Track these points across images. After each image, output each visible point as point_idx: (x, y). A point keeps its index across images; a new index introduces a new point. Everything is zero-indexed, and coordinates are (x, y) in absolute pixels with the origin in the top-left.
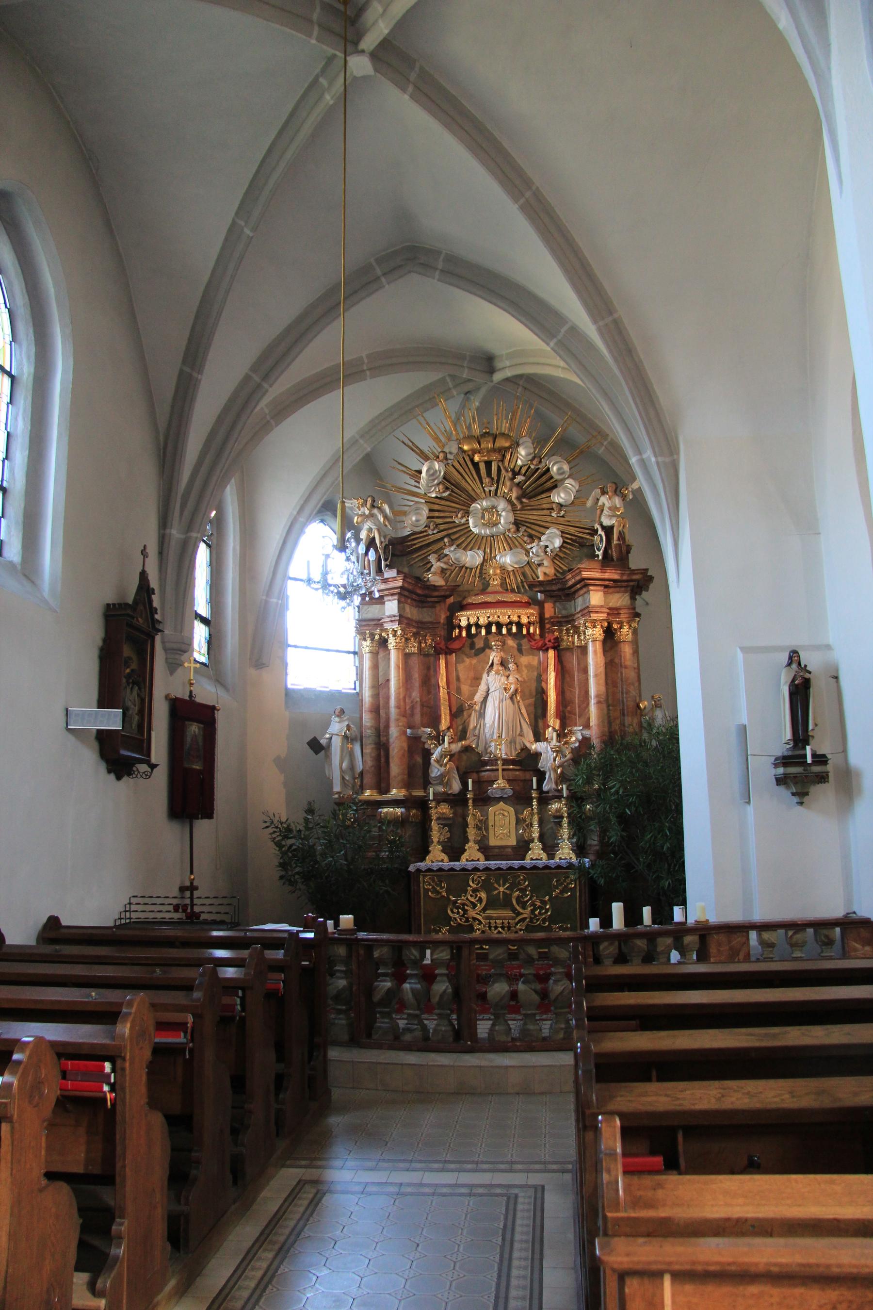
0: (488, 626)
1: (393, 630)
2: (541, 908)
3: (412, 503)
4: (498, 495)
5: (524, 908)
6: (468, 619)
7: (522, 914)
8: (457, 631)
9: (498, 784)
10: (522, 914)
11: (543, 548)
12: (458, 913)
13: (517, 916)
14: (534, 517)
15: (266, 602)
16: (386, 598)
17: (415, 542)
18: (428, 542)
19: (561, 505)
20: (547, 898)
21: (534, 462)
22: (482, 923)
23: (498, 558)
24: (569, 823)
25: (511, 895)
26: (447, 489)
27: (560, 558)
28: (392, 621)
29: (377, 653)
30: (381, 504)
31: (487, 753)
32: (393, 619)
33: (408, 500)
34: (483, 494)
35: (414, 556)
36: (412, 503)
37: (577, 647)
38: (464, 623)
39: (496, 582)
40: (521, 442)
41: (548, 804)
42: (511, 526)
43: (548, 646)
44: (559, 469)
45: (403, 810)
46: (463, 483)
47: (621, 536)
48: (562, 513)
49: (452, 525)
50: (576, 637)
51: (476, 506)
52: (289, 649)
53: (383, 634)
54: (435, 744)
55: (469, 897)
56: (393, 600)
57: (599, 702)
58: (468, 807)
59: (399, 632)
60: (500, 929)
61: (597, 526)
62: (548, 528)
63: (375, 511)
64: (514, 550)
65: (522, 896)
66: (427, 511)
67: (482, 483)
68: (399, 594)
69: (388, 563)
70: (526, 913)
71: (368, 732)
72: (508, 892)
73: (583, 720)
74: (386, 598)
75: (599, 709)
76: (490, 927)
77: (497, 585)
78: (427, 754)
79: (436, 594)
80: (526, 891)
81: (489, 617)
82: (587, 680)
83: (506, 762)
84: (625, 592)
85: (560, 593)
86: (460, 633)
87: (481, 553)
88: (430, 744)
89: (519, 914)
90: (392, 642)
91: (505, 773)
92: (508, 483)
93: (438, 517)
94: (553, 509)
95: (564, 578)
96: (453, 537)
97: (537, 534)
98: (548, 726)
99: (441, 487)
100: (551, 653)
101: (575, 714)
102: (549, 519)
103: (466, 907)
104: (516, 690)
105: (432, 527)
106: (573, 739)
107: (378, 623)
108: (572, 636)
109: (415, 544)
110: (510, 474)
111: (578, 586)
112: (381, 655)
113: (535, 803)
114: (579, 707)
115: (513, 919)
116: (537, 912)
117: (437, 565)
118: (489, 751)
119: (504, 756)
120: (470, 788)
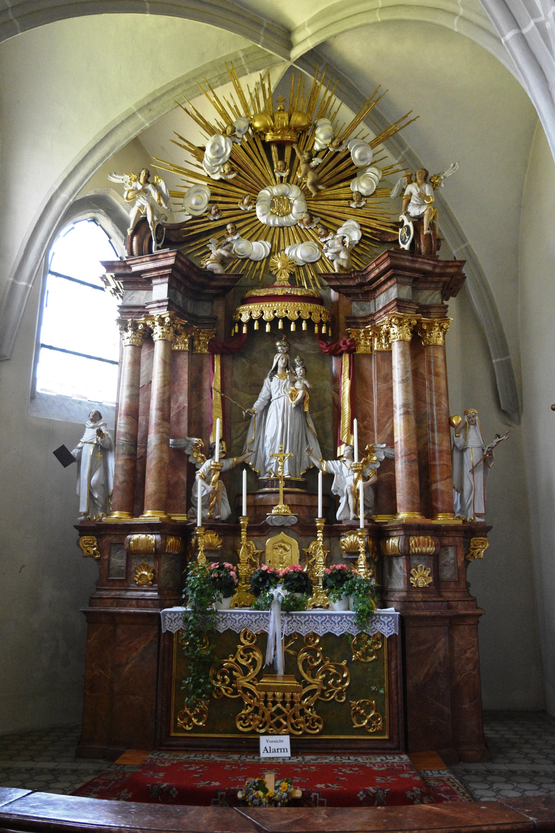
0: (274, 322)
1: (160, 317)
2: (336, 676)
3: (191, 185)
4: (291, 181)
5: (313, 676)
6: (251, 313)
7: (311, 684)
8: (237, 327)
9: (278, 509)
10: (311, 684)
11: (340, 240)
12: (224, 681)
13: (304, 688)
14: (330, 208)
15: (14, 286)
16: (154, 282)
17: (191, 228)
18: (207, 229)
19: (361, 196)
20: (344, 663)
21: (334, 144)
22: (255, 696)
23: (287, 252)
24: (368, 560)
25: (296, 656)
26: (232, 170)
27: (358, 254)
28: (159, 307)
29: (141, 347)
30: (157, 180)
31: (266, 473)
32: (161, 304)
33: (188, 182)
34: (273, 180)
35: (191, 245)
36: (191, 185)
37: (377, 351)
38: (245, 318)
39: (284, 276)
40: (318, 124)
41: (340, 537)
42: (304, 215)
43: (343, 349)
44: (360, 155)
45: (158, 537)
46: (251, 166)
47: (432, 226)
48: (363, 203)
49: (237, 212)
50: (376, 339)
51: (265, 193)
52: (43, 351)
53: (149, 323)
54: (202, 458)
55: (240, 660)
56: (162, 283)
57: (406, 413)
58: (240, 536)
59: (167, 320)
60: (279, 705)
61: (403, 217)
62: (345, 221)
63: (150, 187)
64: (306, 243)
65: (311, 659)
66: (209, 194)
67: (273, 168)
68: (169, 275)
69: (160, 245)
70: (316, 682)
71: (121, 439)
72: (291, 652)
73: (384, 436)
74: (154, 282)
75: (407, 421)
76: (266, 702)
77: (284, 280)
78: (192, 469)
79: (214, 283)
80: (316, 652)
81: (275, 312)
82: (391, 389)
83: (288, 482)
84: (436, 289)
85: (358, 291)
86: (241, 329)
87: (268, 244)
88: (196, 456)
89: (306, 684)
90: (158, 332)
91: (288, 496)
92: (303, 167)
93: (221, 202)
94: (352, 199)
95: (366, 269)
96: (238, 225)
97: (332, 227)
98: (341, 443)
99: (226, 167)
100: (346, 359)
101: (373, 430)
102: (347, 210)
103: (234, 673)
104: (304, 398)
105: (213, 212)
106: (375, 458)
107: (142, 310)
108: (371, 340)
109: (193, 230)
110: (306, 156)
111: (382, 279)
112: (145, 352)
113: (320, 535)
114: (378, 420)
115: (298, 690)
116: (330, 682)
117: (216, 252)
118: (268, 469)
119: (286, 475)
120: (244, 513)
